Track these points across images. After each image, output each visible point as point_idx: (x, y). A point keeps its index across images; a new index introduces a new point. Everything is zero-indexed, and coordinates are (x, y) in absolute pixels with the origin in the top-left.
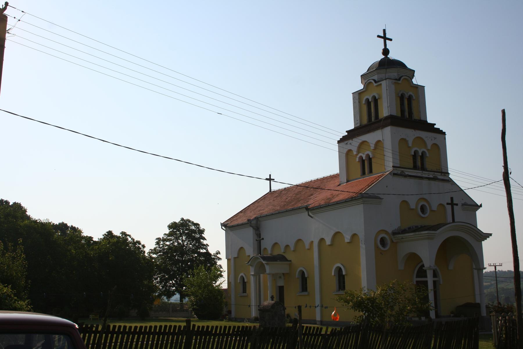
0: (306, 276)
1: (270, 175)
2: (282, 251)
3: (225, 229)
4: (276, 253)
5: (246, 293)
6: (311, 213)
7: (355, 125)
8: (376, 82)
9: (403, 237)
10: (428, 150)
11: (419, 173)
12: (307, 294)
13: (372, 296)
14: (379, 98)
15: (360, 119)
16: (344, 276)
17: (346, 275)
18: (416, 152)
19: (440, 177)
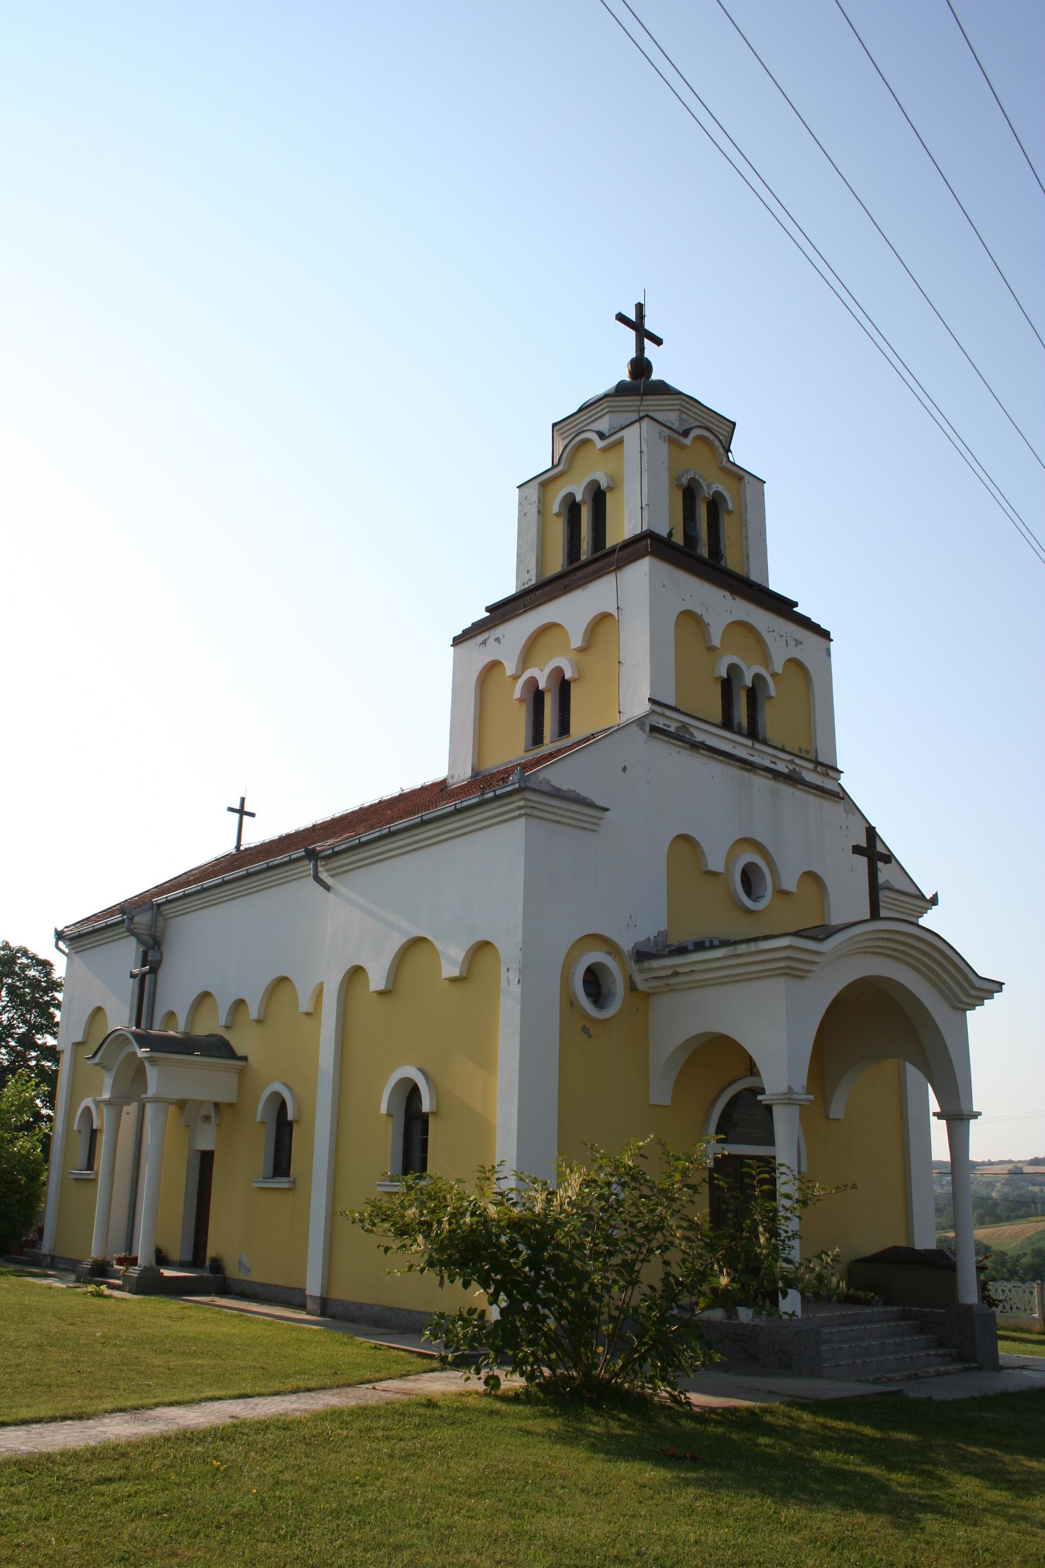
0: (290, 1117)
1: (243, 800)
2: (222, 1021)
3: (67, 950)
4: (203, 1029)
5: (287, 1174)
6: (327, 871)
7: (517, 587)
8: (602, 436)
9: (680, 970)
10: (774, 675)
11: (740, 746)
12: (286, 1186)
13: (537, 1210)
14: (610, 488)
15: (537, 566)
16: (424, 1119)
17: (434, 1113)
18: (734, 669)
19: (810, 777)
